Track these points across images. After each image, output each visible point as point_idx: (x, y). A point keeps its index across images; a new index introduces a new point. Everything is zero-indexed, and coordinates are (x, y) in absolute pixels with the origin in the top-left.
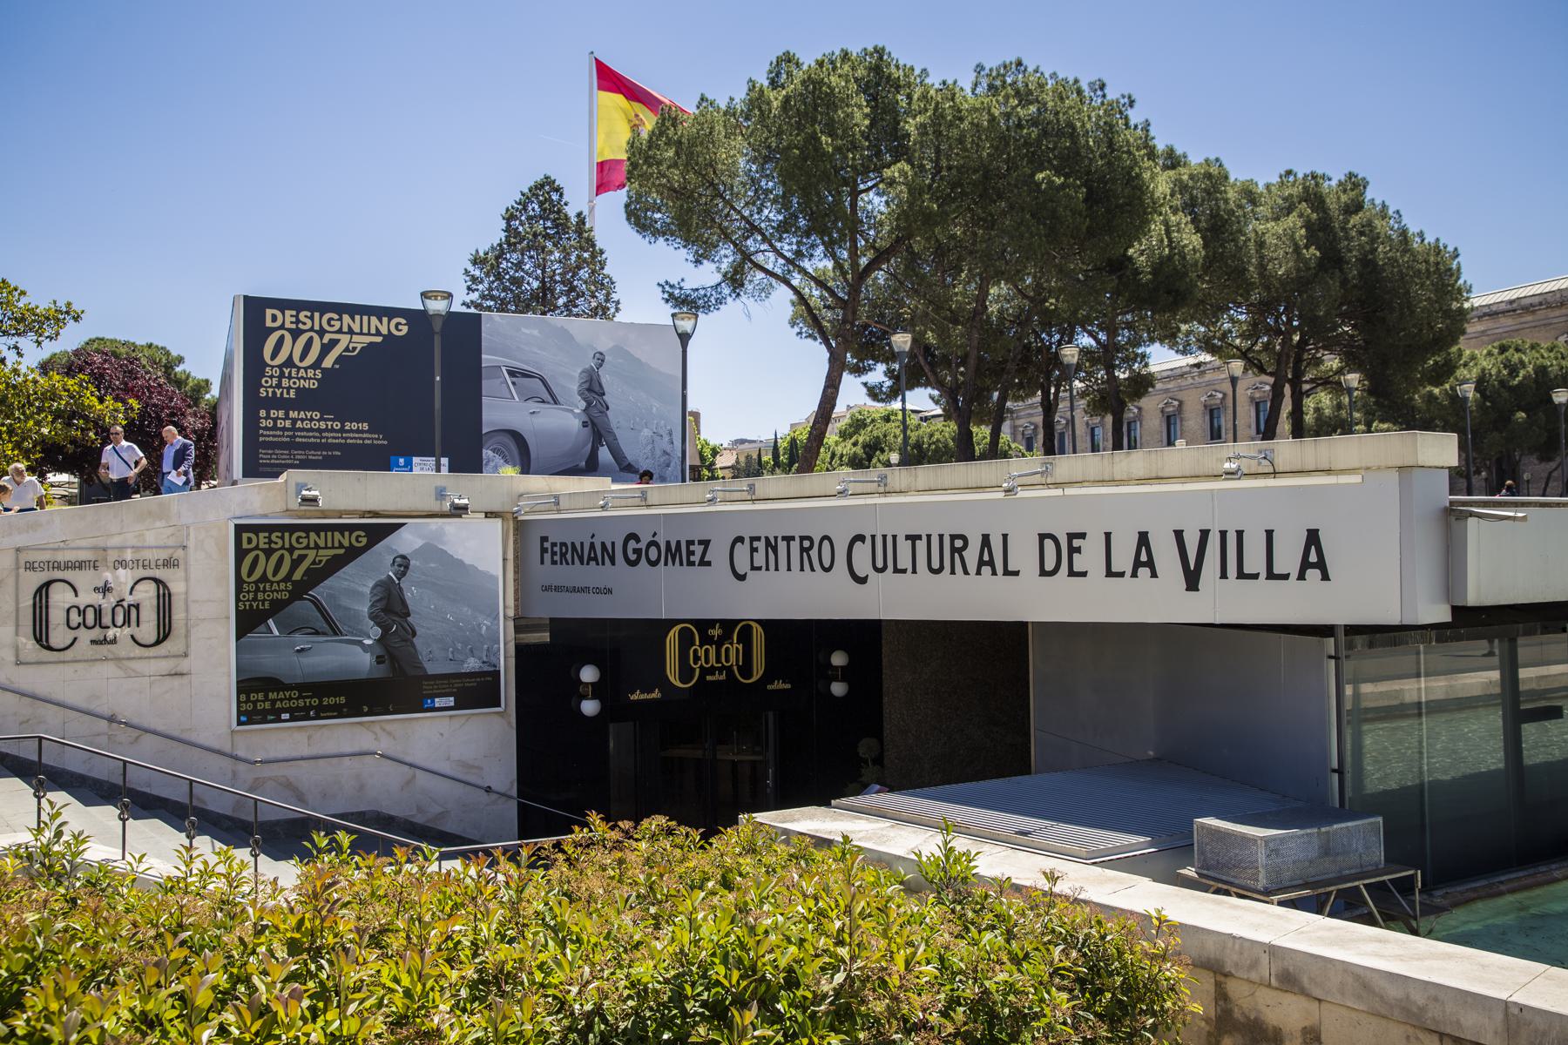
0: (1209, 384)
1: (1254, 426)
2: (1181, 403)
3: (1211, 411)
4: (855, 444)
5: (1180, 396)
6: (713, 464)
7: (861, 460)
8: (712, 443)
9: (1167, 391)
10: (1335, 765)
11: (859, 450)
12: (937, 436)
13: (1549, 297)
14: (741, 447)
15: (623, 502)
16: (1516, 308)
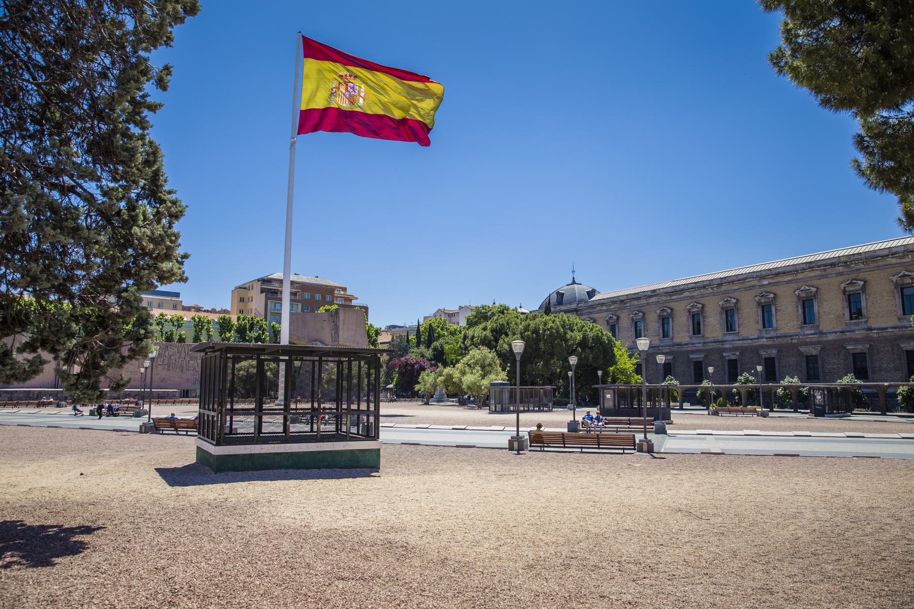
0: (725, 292)
1: (761, 322)
2: (703, 306)
3: (663, 320)
4: (485, 329)
5: (703, 301)
6: (375, 340)
7: (490, 341)
8: (376, 326)
9: (692, 297)
10: (236, 406)
11: (488, 333)
12: (550, 324)
13: (797, 267)
14: (393, 330)
16: (613, 301)
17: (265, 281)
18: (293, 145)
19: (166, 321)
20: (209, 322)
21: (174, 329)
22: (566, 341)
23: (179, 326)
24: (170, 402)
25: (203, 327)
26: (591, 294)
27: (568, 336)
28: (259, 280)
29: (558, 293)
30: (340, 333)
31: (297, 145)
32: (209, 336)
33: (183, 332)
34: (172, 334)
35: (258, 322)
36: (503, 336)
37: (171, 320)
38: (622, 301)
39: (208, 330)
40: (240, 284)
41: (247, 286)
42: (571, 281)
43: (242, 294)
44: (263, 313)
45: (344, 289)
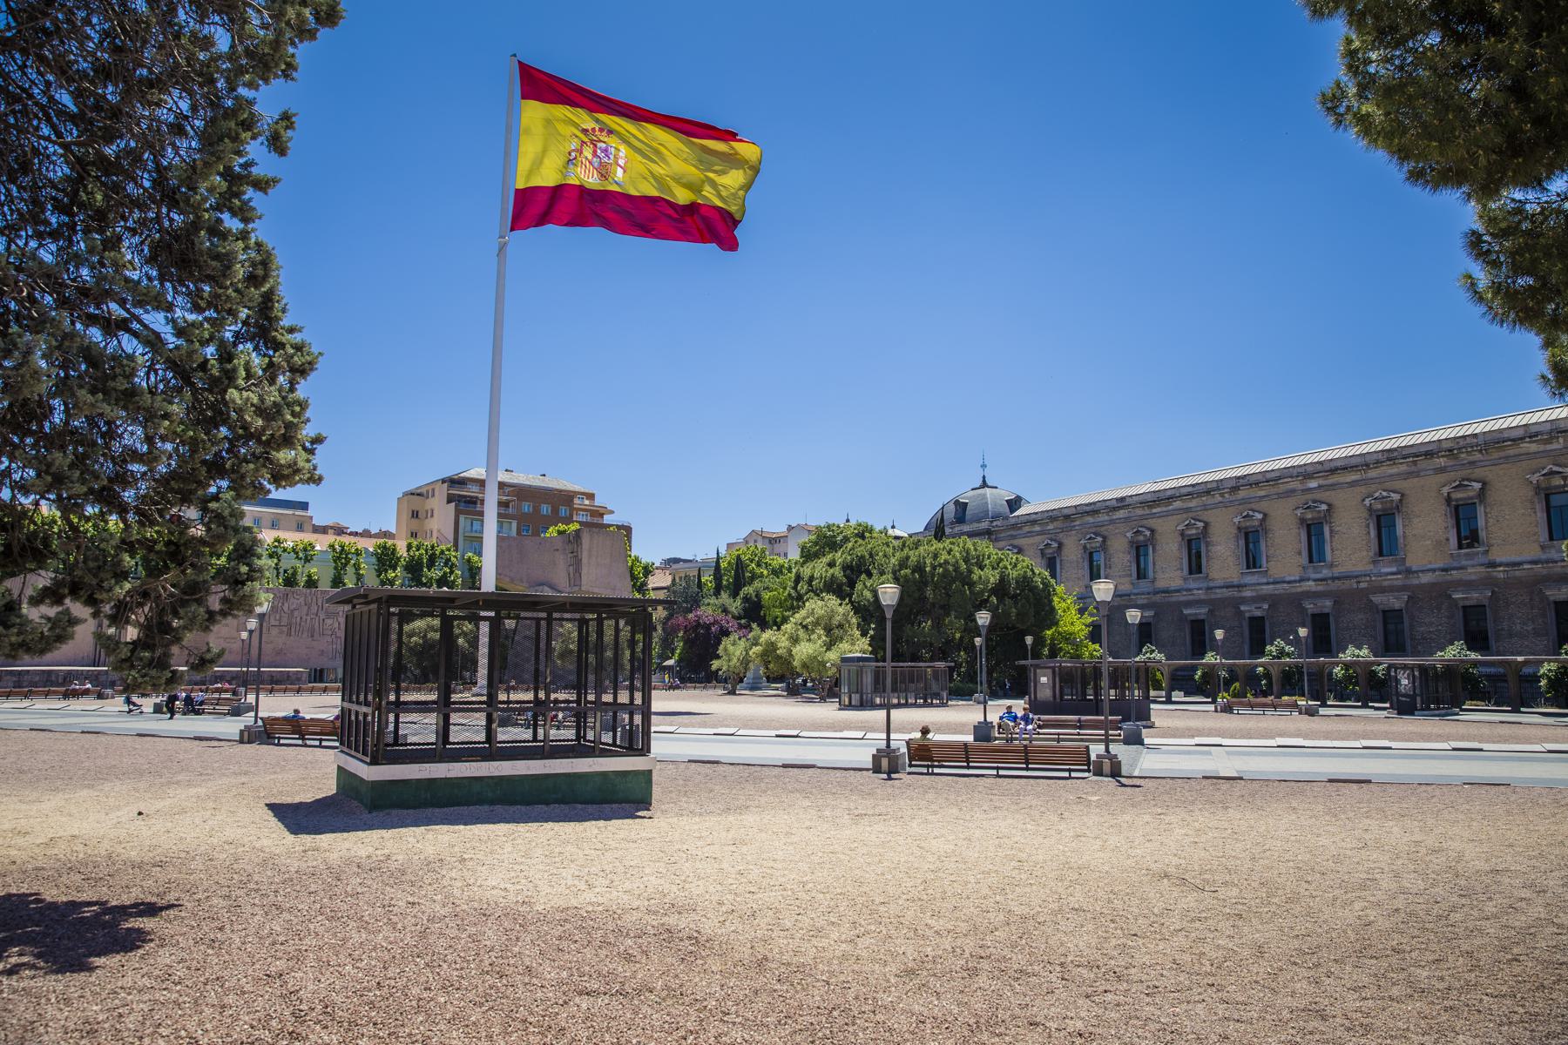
0: (1244, 501)
1: (1305, 553)
2: (1207, 525)
3: (1138, 548)
4: (831, 564)
5: (1206, 516)
6: (644, 584)
7: (840, 586)
8: (645, 559)
9: (1188, 510)
10: (405, 697)
11: (837, 571)
12: (944, 557)
13: (1368, 458)
14: (675, 566)
15: (365, 640)
16: (1052, 516)
17: (455, 482)
18: (502, 248)
19: (285, 550)
20: (358, 553)
21: (299, 564)
22: (971, 584)
23: (307, 560)
24: (291, 690)
25: (348, 561)
26: (1014, 504)
27: (975, 577)
28: (444, 481)
29: (957, 503)
30: (584, 572)
31: (509, 249)
32: (359, 577)
33: (314, 570)
34: (295, 573)
35: (442, 552)
36: (863, 576)
37: (294, 550)
38: (1067, 517)
39: (357, 567)
40: (411, 487)
41: (424, 491)
42: (979, 483)
43: (415, 505)
44: (451, 537)
45: (591, 496)
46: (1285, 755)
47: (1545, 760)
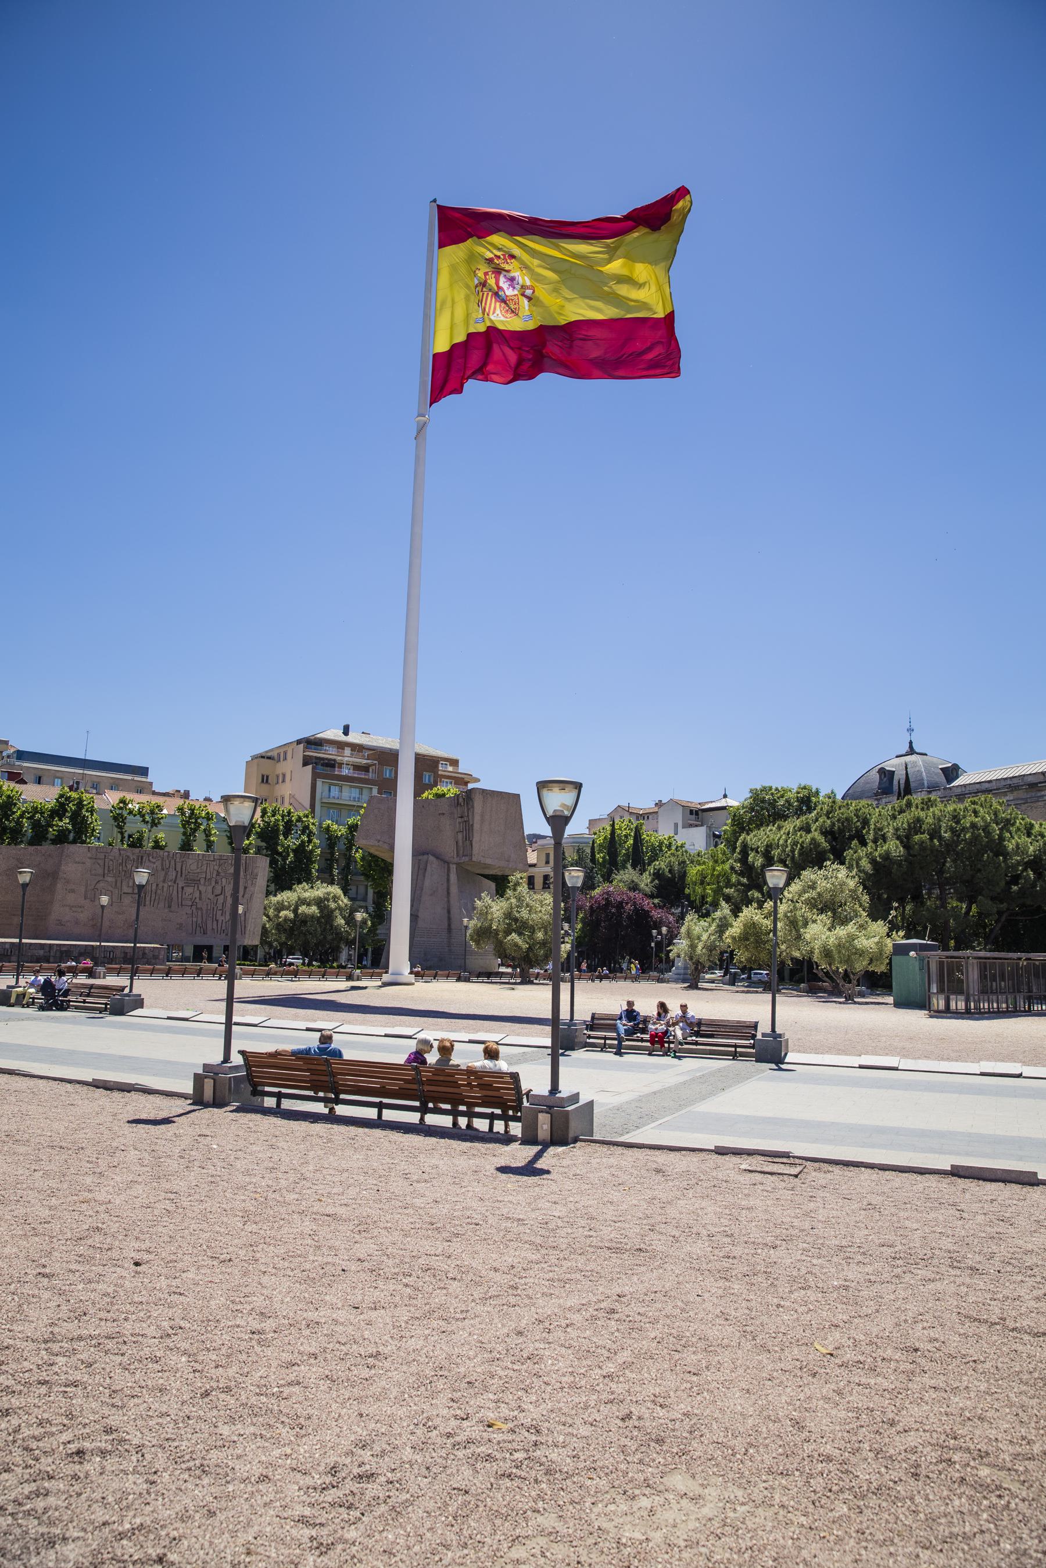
17: (312, 742)
18: (421, 428)
19: (131, 812)
20: (209, 817)
21: (145, 829)
22: (1006, 854)
23: (155, 823)
24: (159, 971)
25: (198, 825)
26: (951, 772)
27: (1010, 846)
28: (299, 742)
29: (882, 772)
30: (476, 838)
31: (429, 430)
32: (210, 845)
33: (161, 835)
34: (140, 839)
35: (299, 819)
36: (855, 842)
37: (140, 812)
38: (1033, 786)
39: (207, 833)
40: (261, 750)
41: (275, 754)
42: (906, 748)
43: (265, 768)
44: (307, 803)
45: (455, 763)
46: (998, 1092)
47: (980, 1091)
